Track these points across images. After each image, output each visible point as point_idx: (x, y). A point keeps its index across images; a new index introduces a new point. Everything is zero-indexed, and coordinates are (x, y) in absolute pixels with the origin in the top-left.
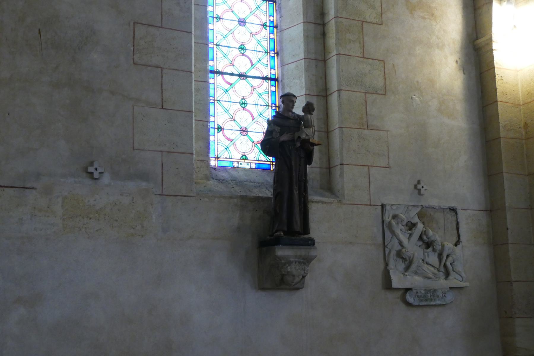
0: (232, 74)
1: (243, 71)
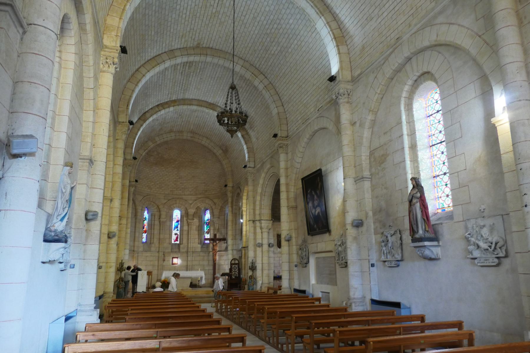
0: (442, 175)
1: (445, 171)
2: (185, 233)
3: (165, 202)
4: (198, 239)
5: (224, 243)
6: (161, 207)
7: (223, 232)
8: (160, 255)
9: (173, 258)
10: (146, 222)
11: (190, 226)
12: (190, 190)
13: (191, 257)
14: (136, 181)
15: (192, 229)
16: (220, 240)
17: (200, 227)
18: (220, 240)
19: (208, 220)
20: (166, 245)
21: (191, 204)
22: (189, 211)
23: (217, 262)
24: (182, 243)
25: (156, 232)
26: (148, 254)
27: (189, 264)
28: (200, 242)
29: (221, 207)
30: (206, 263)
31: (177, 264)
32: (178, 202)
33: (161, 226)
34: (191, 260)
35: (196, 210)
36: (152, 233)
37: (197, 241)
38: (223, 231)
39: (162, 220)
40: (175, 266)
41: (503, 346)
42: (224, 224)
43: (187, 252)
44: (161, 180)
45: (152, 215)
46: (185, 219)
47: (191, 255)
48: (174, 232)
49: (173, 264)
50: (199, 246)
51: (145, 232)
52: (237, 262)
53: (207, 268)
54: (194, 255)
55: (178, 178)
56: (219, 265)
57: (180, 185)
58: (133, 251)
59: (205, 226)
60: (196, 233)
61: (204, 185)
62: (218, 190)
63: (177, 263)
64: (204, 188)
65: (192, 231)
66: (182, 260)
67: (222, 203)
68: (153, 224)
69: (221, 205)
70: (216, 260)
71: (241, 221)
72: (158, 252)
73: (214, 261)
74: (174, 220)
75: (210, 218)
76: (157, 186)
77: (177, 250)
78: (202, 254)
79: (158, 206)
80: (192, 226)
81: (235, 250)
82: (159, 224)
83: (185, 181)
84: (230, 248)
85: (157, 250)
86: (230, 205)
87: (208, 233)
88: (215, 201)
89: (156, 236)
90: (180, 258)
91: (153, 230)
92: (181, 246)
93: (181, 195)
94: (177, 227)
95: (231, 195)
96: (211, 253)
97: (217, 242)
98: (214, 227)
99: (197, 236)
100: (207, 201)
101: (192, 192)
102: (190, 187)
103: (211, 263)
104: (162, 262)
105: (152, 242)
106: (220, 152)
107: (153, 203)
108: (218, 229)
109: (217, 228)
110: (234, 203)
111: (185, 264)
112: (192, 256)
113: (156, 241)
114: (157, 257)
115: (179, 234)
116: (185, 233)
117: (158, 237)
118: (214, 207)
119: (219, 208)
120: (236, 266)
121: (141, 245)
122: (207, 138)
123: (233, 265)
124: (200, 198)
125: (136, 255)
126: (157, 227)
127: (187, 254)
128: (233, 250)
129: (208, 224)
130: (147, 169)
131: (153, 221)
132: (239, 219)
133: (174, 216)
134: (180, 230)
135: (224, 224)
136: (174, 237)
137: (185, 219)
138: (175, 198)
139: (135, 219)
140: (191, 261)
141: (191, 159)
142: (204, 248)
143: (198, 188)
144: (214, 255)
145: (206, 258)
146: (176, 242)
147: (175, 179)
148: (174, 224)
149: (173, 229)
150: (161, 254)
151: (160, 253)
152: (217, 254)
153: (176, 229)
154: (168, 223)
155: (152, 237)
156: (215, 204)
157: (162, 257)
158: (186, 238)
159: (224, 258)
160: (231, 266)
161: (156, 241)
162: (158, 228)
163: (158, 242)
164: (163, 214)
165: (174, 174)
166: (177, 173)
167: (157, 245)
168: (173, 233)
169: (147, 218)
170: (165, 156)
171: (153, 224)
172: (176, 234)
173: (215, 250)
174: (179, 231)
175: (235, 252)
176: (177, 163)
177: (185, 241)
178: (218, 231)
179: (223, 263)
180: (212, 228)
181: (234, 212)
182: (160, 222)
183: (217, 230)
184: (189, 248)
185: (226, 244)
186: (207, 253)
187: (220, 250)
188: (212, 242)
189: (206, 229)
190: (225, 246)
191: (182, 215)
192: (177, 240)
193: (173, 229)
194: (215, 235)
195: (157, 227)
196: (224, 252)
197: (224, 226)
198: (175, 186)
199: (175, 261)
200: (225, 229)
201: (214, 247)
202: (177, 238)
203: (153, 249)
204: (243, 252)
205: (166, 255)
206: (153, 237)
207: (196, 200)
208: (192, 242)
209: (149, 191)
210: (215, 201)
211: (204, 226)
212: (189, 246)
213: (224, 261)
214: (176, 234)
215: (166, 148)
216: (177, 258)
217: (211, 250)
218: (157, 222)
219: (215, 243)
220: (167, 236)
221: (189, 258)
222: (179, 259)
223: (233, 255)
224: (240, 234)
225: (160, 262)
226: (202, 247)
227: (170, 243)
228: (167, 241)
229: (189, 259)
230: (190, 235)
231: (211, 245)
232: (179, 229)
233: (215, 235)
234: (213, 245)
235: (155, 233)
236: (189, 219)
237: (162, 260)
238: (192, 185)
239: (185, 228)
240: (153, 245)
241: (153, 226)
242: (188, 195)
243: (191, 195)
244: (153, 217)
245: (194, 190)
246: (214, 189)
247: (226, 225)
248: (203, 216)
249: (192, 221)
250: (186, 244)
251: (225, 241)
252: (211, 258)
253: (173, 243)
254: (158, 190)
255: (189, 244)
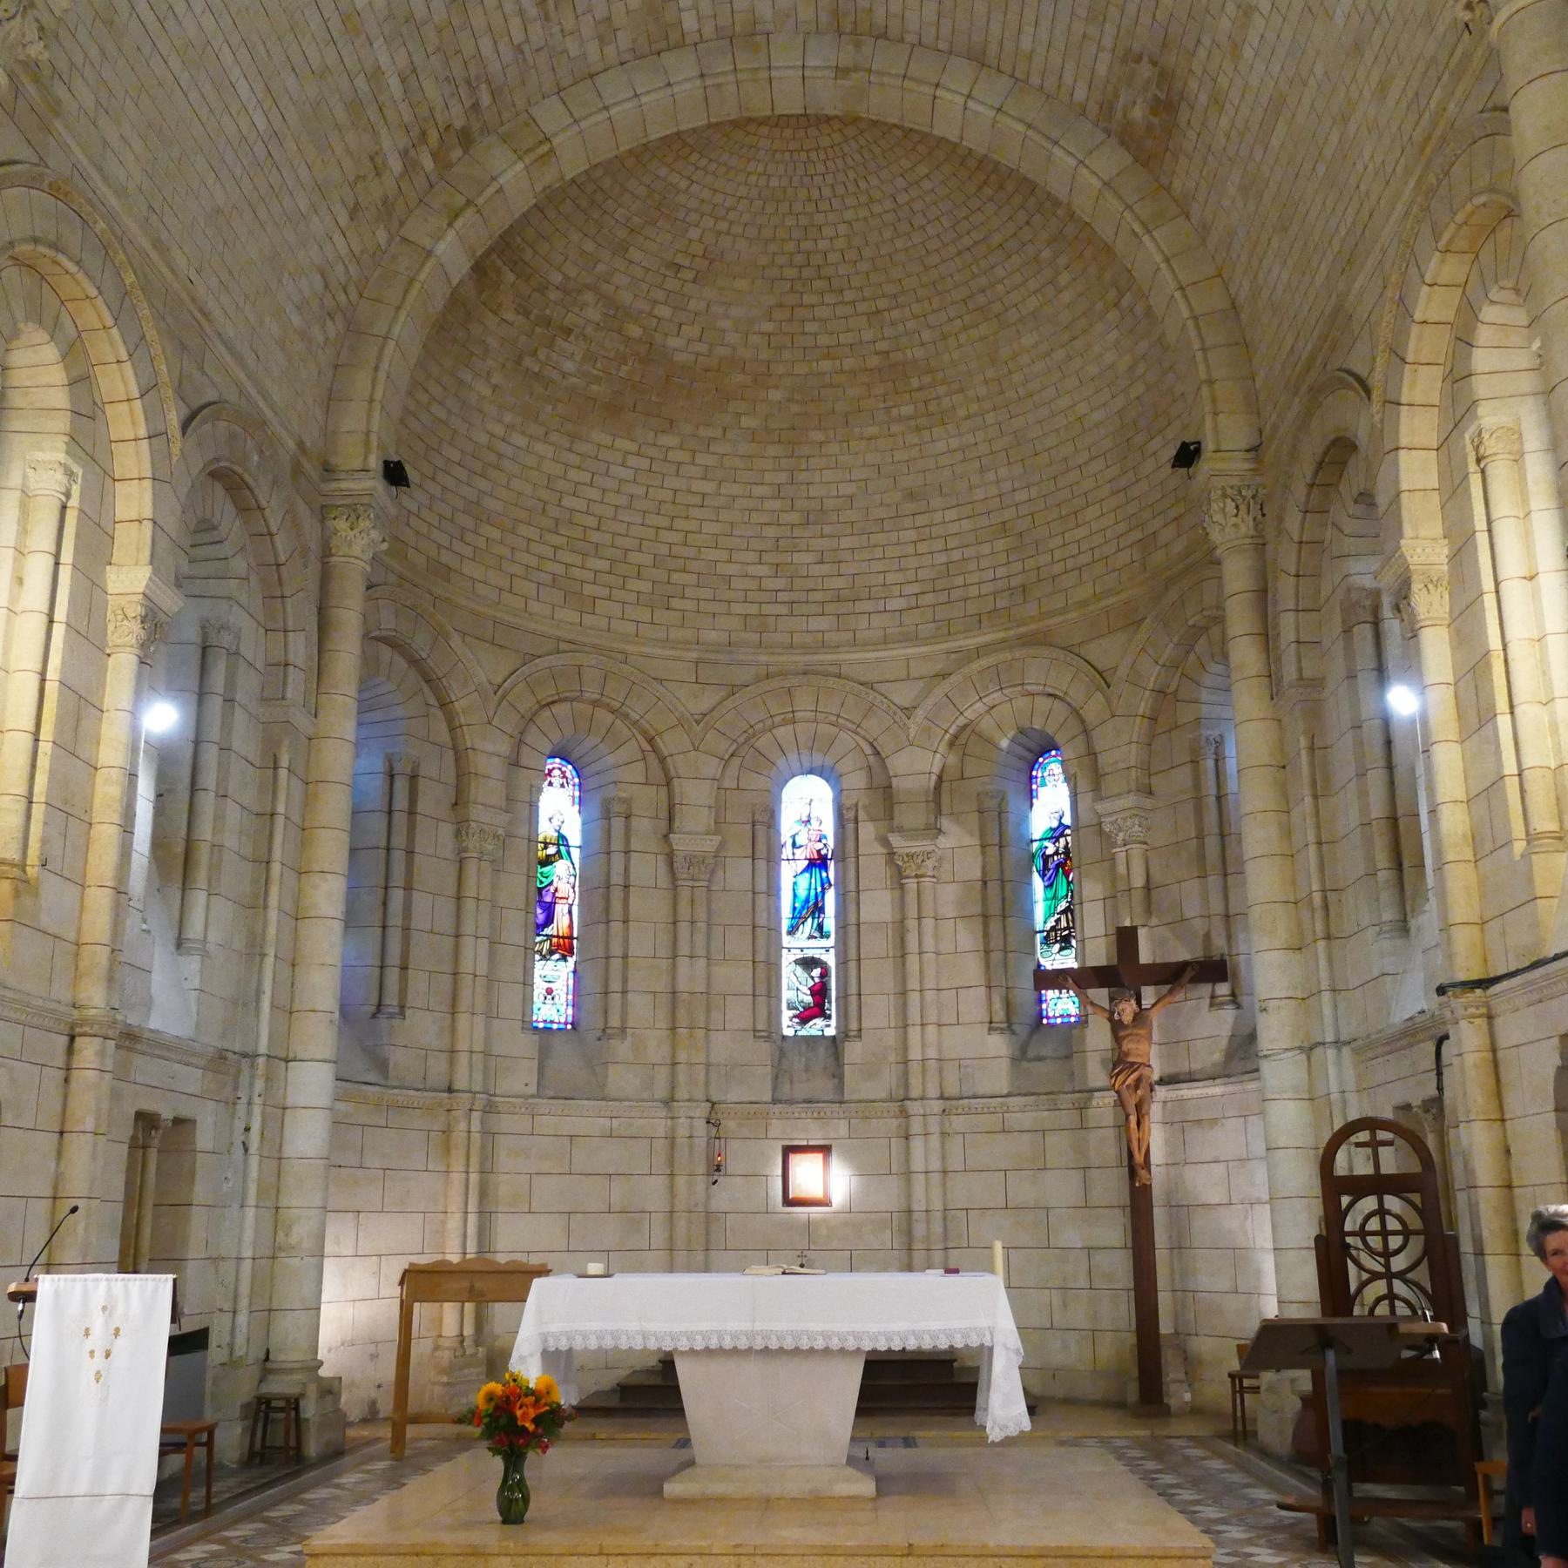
2: (876, 945)
3: (705, 705)
4: (982, 992)
5: (1214, 1002)
6: (670, 743)
7: (1192, 909)
8: (682, 1131)
9: (788, 1151)
10: (563, 877)
11: (911, 884)
12: (896, 604)
13: (935, 1141)
14: (395, 474)
15: (928, 910)
16: (1172, 976)
17: (994, 888)
18: (1172, 976)
19: (1056, 834)
20: (722, 1046)
21: (908, 711)
22: (900, 763)
23: (1158, 1178)
24: (854, 1026)
25: (644, 940)
26: (585, 1119)
27: (918, 1205)
28: (1000, 1015)
29: (1161, 692)
30: (1060, 1188)
31: (825, 1202)
32: (804, 702)
33: (685, 895)
34: (936, 1164)
35: (952, 760)
36: (616, 950)
37: (974, 1004)
38: (1192, 897)
39: (680, 843)
40: (809, 1224)
41: (391, 1066)
42: (1200, 837)
43: (903, 1099)
44: (666, 536)
45: (607, 815)
46: (868, 831)
47: (934, 1127)
48: (797, 944)
49: (788, 1202)
50: (998, 1045)
51: (563, 947)
52: (1391, 1161)
53: (1072, 1237)
54: (958, 1123)
55: (794, 517)
56: (1182, 1210)
57: (818, 570)
58: (450, 1090)
59: (1038, 883)
60: (967, 938)
61: (1001, 545)
62: (1124, 557)
63: (816, 1192)
64: (1001, 572)
65: (928, 923)
66: (864, 1171)
67: (1168, 652)
68: (617, 879)
69: (1152, 674)
70: (1147, 1164)
71: (1402, 700)
72: (669, 1101)
73: (1135, 1167)
74: (787, 852)
75: (1067, 821)
76: (633, 584)
77: (822, 1086)
78: (1024, 1115)
79: (651, 741)
80: (927, 882)
81: (1338, 1044)
82: (663, 881)
83: (846, 542)
84: (1275, 1031)
85: (661, 1091)
86: (1245, 654)
87: (1061, 937)
88: (1105, 651)
89: (646, 979)
90: (851, 1158)
91: (616, 927)
92: (853, 1052)
93: (823, 646)
94: (818, 909)
95: (1246, 526)
96: (1104, 1103)
97: (1149, 994)
98: (1113, 876)
99: (972, 970)
100: (1039, 670)
101: (910, 619)
102: (891, 578)
103: (1111, 1187)
104: (700, 1183)
105: (615, 1021)
106: (1111, 160)
107: (610, 718)
108: (1148, 888)
109: (1138, 881)
110: (1286, 589)
111: (888, 1197)
112: (944, 1134)
113: (642, 1009)
114: (660, 1145)
115: (830, 959)
116: (876, 945)
117: (662, 984)
118: (1093, 709)
119: (1144, 706)
120: (1392, 1203)
121: (526, 1045)
122: (978, 58)
123: (1358, 1196)
124: (979, 652)
125: (467, 1127)
126: (648, 906)
127: (904, 1114)
128: (1309, 1049)
129: (1058, 867)
130: (539, 447)
131: (618, 862)
132: (1381, 675)
133: (788, 825)
134: (842, 927)
135: (1200, 837)
136: (794, 986)
137: (868, 831)
138: (784, 674)
139: (458, 834)
140: (936, 1178)
141: (881, 346)
142: (1040, 1059)
143: (959, 581)
144: (1132, 1113)
145: (1058, 1144)
146: (816, 1027)
147: (770, 532)
148: (793, 881)
149: (785, 924)
150: (692, 1120)
151: (681, 1109)
152: (1155, 1111)
153: (808, 927)
154: (737, 873)
155: (616, 985)
156: (1103, 679)
157: (701, 1143)
158: (890, 984)
159: (1227, 1139)
160: (1333, 1217)
161: (642, 1009)
162: (662, 911)
163: (663, 1021)
164: (695, 794)
165: (759, 491)
166: (782, 477)
167: (656, 1047)
168: (787, 960)
169: (575, 838)
170: (674, 342)
171: (617, 879)
172: (808, 963)
173: (1133, 1067)
174: (831, 942)
175: (1338, 1072)
176: (776, 395)
177: (878, 1012)
178: (1149, 911)
179: (1214, 1195)
180: (1093, 889)
181: (1290, 673)
182: (670, 858)
183: (1138, 896)
184: (915, 1068)
185: (1229, 1014)
186: (1065, 1100)
187: (1172, 1070)
188: (1100, 995)
189: (1042, 906)
190: (1226, 1031)
191: (848, 802)
192: (816, 1010)
193: (785, 924)
194: (1126, 939)
195: (648, 906)
196: (1216, 1089)
197: (1201, 857)
198: (780, 583)
199: (808, 1174)
200: (1214, 881)
201: (1126, 1045)
202: (820, 992)
203: (622, 1079)
204: (1468, 1040)
205: (730, 1125)
206: (625, 980)
207: (944, 676)
208: (932, 1016)
209: (574, 617)
210: (1105, 651)
211: (1030, 884)
212: (915, 1053)
213: (1219, 1169)
214: (808, 963)
215: (679, 267)
216: (825, 1150)
217: (1097, 1075)
218: (647, 869)
219: (1127, 1010)
220: (735, 976)
221: (917, 1145)
222: (835, 1161)
223: (1313, 1098)
224: (1384, 875)
225: (681, 1182)
226: (1021, 1056)
227: (770, 1032)
228: (738, 1014)
229: (918, 1164)
230: (913, 962)
231: (1098, 1036)
232: (830, 924)
233: (1126, 939)
234: (1116, 1027)
235: (633, 950)
236: (900, 830)
237: (701, 1168)
238: (913, 562)
239: (878, 906)
240: (622, 1049)
241: (616, 894)
242: (885, 641)
243: (906, 639)
244: (618, 824)
245: (928, 599)
246: (1085, 558)
247: (1212, 844)
248: (1014, 803)
249: (918, 846)
250: (891, 1038)
251: (1223, 989)
252: (1103, 1145)
253: (789, 1032)
254: (644, 614)
255: (914, 1034)
